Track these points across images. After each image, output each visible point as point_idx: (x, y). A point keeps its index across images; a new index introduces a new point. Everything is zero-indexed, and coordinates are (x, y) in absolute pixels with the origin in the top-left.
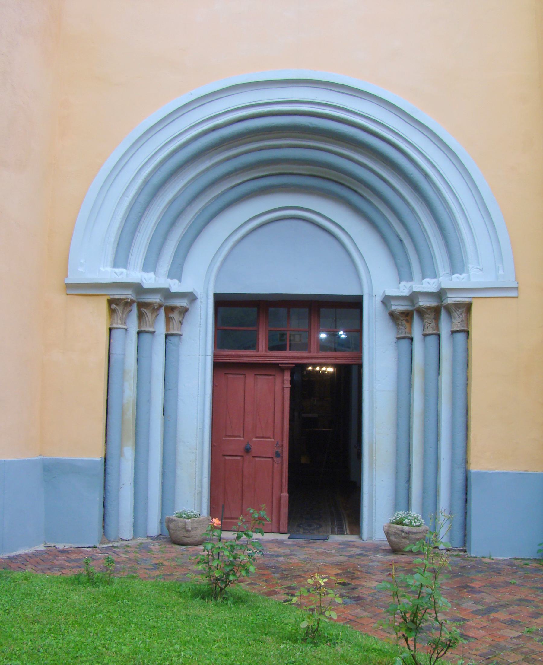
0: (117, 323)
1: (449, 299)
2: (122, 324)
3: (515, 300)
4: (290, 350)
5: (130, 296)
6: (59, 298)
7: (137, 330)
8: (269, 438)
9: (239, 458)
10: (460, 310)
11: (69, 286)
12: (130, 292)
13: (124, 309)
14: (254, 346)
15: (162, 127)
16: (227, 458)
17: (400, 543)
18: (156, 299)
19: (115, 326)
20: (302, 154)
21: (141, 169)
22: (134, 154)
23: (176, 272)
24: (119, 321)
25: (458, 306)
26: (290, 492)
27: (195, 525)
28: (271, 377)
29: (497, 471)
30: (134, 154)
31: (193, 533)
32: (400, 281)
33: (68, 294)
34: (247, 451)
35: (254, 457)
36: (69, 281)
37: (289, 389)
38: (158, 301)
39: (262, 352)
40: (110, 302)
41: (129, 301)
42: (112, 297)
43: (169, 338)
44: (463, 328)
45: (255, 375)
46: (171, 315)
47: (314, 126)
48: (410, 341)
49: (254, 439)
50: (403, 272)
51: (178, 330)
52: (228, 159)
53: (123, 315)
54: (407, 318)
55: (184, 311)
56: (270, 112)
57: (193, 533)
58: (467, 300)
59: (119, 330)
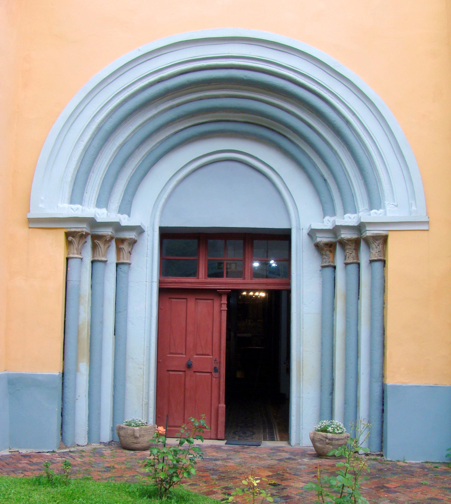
0: (73, 254)
1: (367, 232)
2: (78, 254)
3: (426, 233)
4: (227, 277)
5: (85, 229)
6: (22, 231)
7: (91, 259)
8: (208, 355)
9: (181, 373)
10: (377, 242)
11: (31, 221)
12: (85, 226)
13: (79, 241)
14: (195, 274)
15: (113, 79)
16: (171, 373)
17: (324, 448)
18: (108, 232)
19: (71, 256)
20: (237, 104)
21: (95, 116)
22: (89, 103)
23: (126, 207)
24: (75, 252)
25: (376, 238)
26: (226, 403)
27: (143, 432)
28: (209, 301)
29: (410, 384)
30: (89, 103)
31: (140, 440)
32: (324, 216)
33: (30, 228)
34: (189, 366)
35: (194, 372)
36: (31, 216)
37: (226, 311)
38: (110, 233)
39: (202, 279)
40: (68, 235)
41: (84, 233)
42: (69, 230)
43: (120, 266)
44: (380, 258)
45: (196, 299)
46: (121, 246)
47: (248, 78)
48: (333, 269)
49: (195, 356)
50: (327, 208)
51: (127, 260)
52: (172, 108)
53: (78, 246)
54: (330, 249)
55: (133, 243)
56: (209, 65)
57: (140, 440)
58: (384, 233)
59: (75, 259)
